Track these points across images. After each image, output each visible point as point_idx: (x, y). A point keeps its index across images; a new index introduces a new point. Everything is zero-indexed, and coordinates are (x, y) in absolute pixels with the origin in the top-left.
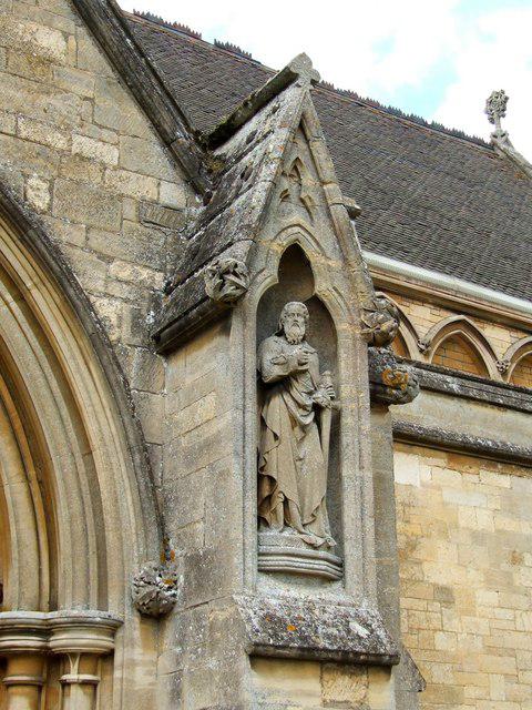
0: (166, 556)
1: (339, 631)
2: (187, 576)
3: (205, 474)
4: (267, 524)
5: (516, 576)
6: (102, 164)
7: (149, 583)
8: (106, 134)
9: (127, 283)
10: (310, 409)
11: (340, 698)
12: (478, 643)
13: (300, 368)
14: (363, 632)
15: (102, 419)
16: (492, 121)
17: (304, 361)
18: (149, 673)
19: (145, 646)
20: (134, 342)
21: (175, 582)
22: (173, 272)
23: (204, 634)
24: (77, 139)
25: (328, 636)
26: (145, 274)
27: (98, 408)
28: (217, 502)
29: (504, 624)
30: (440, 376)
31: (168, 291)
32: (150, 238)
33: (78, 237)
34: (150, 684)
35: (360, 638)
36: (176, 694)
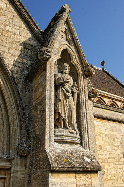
0: (28, 137)
1: (81, 161)
2: (33, 143)
3: (39, 112)
4: (58, 127)
5: (114, 143)
6: (14, 33)
7: (22, 146)
8: (16, 27)
9: (20, 62)
10: (70, 92)
11: (82, 184)
12: (107, 157)
13: (67, 80)
14: (89, 160)
15: (10, 98)
16: (102, 66)
17: (68, 79)
18: (22, 174)
19: (21, 166)
20: (21, 77)
21: (30, 146)
22: (33, 61)
23: (37, 162)
24: (7, 27)
25: (78, 162)
26: (25, 61)
27: (9, 95)
28: (41, 120)
29: (112, 153)
30: (98, 104)
31: (31, 65)
32: (27, 52)
33: (6, 50)
34: (23, 178)
35: (88, 162)
36: (29, 182)
